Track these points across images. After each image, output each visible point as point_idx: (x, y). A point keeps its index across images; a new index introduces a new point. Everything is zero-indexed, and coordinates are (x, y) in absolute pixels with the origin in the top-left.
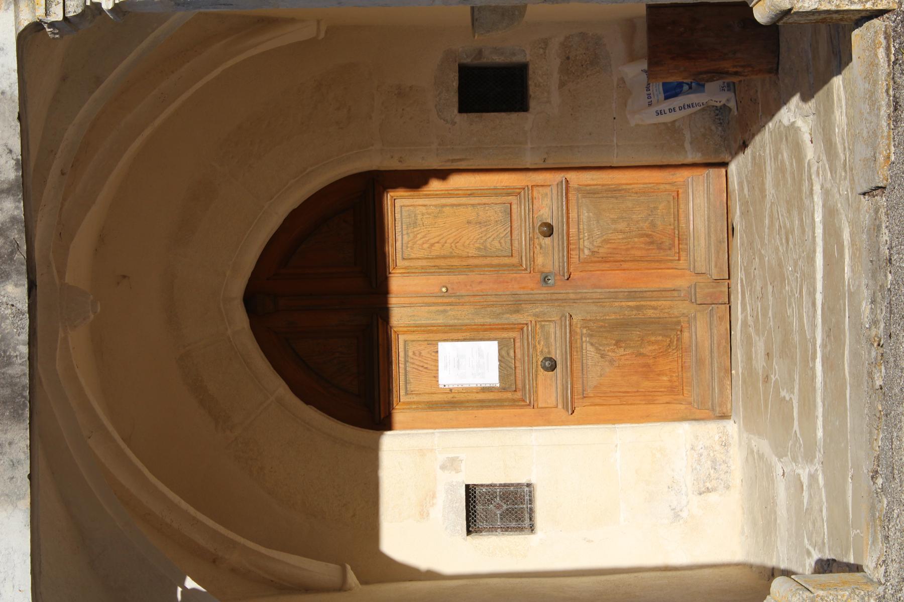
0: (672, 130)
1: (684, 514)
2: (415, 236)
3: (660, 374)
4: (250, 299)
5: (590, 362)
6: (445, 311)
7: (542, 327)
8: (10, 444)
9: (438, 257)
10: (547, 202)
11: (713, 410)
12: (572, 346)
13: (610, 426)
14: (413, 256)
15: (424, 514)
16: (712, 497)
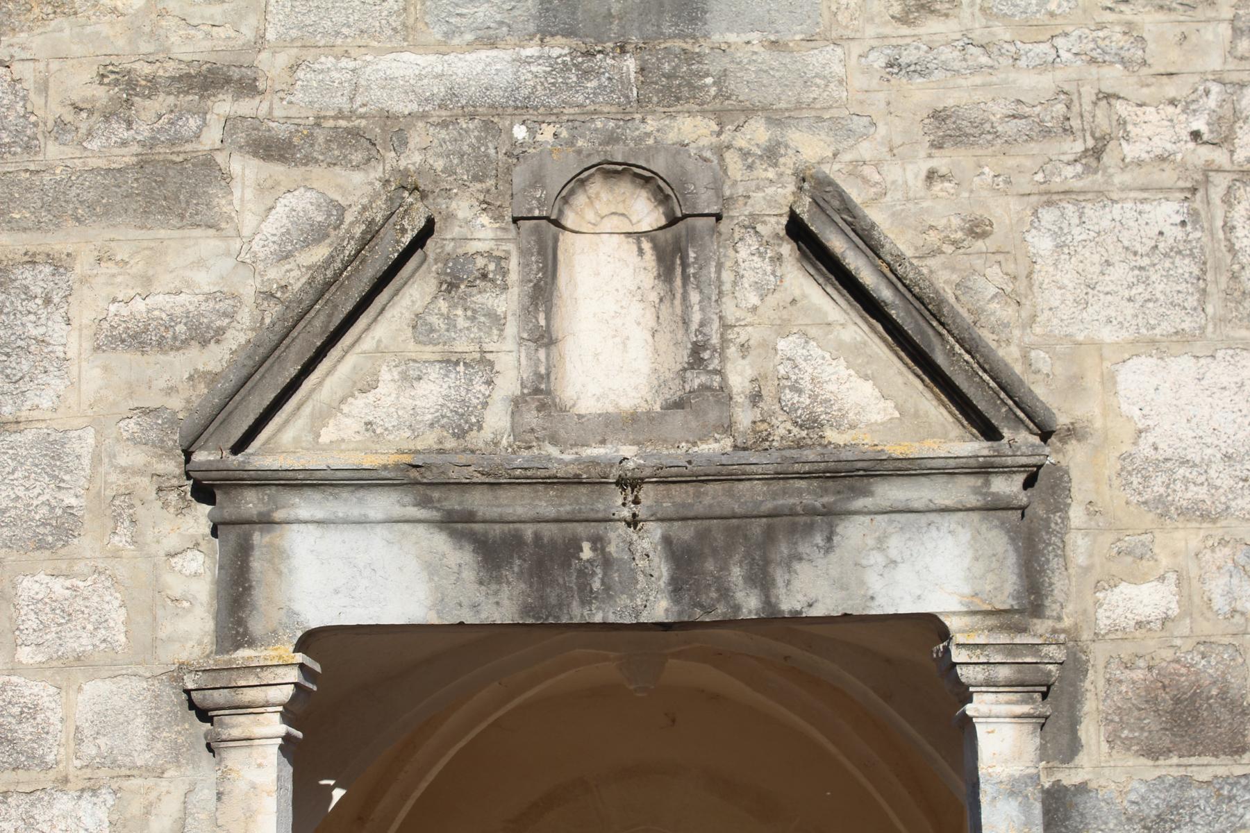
8: (497, 603)
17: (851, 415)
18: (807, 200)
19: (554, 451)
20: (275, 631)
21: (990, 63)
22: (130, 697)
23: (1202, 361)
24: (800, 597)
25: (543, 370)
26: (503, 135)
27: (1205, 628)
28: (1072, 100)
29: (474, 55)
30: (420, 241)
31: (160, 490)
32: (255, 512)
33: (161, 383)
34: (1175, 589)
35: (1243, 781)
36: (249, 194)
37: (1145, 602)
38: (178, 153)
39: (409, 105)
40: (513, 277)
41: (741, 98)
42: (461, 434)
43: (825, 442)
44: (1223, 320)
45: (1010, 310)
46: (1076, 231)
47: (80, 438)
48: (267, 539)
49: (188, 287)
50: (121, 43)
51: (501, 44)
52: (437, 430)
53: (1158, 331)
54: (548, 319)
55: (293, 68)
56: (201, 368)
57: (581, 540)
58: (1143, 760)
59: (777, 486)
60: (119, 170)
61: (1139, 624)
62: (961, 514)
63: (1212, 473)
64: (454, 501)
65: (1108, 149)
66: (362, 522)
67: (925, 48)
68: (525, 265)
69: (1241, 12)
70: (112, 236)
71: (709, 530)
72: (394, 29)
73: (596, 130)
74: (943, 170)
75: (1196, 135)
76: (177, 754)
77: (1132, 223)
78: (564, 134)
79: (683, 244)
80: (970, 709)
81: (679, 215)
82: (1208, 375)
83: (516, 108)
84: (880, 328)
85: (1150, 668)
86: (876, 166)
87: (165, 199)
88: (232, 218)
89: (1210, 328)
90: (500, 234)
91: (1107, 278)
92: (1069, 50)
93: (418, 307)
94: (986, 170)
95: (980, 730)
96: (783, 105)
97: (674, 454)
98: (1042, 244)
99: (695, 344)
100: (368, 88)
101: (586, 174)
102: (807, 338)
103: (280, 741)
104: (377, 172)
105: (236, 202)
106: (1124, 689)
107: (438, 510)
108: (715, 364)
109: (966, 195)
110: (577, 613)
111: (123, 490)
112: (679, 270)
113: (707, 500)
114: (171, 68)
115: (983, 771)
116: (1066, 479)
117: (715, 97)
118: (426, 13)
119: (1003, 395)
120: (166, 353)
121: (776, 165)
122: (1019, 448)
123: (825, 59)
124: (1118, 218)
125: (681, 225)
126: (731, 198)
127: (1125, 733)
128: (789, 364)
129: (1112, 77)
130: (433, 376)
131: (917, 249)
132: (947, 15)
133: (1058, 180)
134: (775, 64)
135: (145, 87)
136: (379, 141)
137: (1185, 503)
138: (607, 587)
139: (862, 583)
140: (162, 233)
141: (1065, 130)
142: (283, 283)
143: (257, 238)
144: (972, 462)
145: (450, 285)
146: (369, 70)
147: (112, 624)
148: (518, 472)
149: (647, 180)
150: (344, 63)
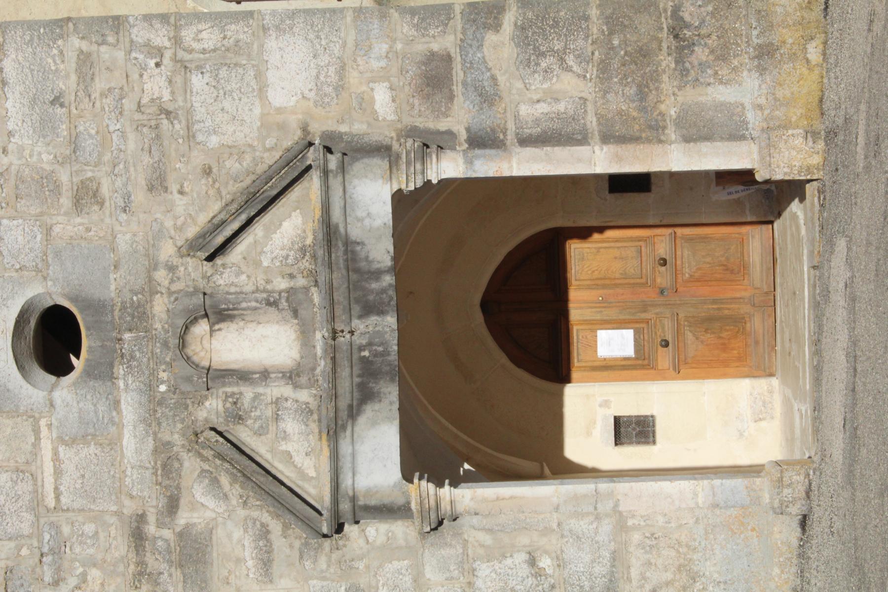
0: (738, 202)
1: (746, 434)
2: (583, 267)
3: (733, 349)
4: (486, 305)
5: (689, 342)
6: (601, 312)
7: (660, 321)
8: (390, 393)
9: (597, 279)
10: (663, 245)
11: (765, 371)
12: (678, 333)
13: (701, 381)
14: (582, 278)
15: (589, 434)
16: (763, 424)
17: (299, 232)
18: (199, 253)
19: (318, 370)
20: (403, 493)
21: (123, 163)
22: (432, 557)
23: (269, 66)
24: (385, 257)
25: (281, 375)
26: (165, 396)
27: (394, 70)
28: (142, 124)
29: (124, 411)
30: (220, 434)
31: (337, 549)
32: (349, 504)
33: (288, 551)
34: (377, 84)
35: (464, 57)
36: (195, 515)
37: (383, 98)
38: (175, 549)
39: (150, 441)
40: (235, 389)
41: (143, 283)
42: (311, 412)
43: (312, 244)
44: (249, 55)
45: (247, 157)
46: (207, 124)
47: (313, 587)
48: (361, 498)
49: (241, 541)
50: (119, 580)
51: (118, 398)
52: (308, 423)
53: (255, 87)
54: (256, 373)
55: (132, 497)
56: (280, 533)
57: (360, 356)
58: (455, 102)
59: (334, 267)
60: (184, 577)
61: (394, 101)
62: (346, 183)
63: (322, 64)
64: (344, 414)
65: (166, 108)
66: (353, 455)
67: (116, 194)
68: (230, 384)
69: (94, 40)
70: (216, 577)
71: (355, 298)
72: (111, 449)
73: (161, 352)
74: (178, 187)
75: (158, 65)
76: (457, 535)
77: (203, 97)
78: (163, 367)
79: (218, 310)
80: (435, 181)
81: (204, 313)
82: (276, 64)
83: (150, 390)
84: (257, 219)
85: (413, 96)
86: (176, 219)
87: (198, 554)
88: (207, 523)
89: (253, 62)
90: (214, 396)
91: (230, 110)
92: (116, 124)
93: (250, 433)
94: (177, 166)
95: (444, 176)
96: (147, 263)
97: (320, 315)
98: (214, 141)
99: (267, 305)
100: (141, 461)
101: (184, 356)
102: (262, 252)
103: (452, 488)
104: (184, 455)
105: (199, 521)
106: (423, 109)
107: (347, 421)
108: (276, 295)
109: (190, 176)
110: (393, 357)
111: (338, 566)
112: (230, 312)
113: (341, 299)
114: (132, 555)
115: (462, 176)
116: (327, 133)
117: (143, 295)
118: (102, 435)
119: (291, 164)
120: (273, 550)
121: (177, 266)
122: (316, 157)
123: (123, 242)
124: (200, 104)
125: (208, 312)
126: (194, 288)
127: (443, 109)
128: (275, 261)
129: (129, 104)
130: (284, 425)
131: (217, 200)
132: (99, 184)
133: (182, 132)
134: (126, 267)
135: (141, 567)
136: (168, 455)
137: (337, 77)
138: (381, 344)
139: (378, 229)
140: (215, 555)
141: (156, 128)
142: (239, 497)
143: (216, 510)
144: (323, 179)
145: (239, 419)
146: (132, 461)
147: (399, 567)
148: (330, 385)
149: (187, 328)
150: (128, 473)
